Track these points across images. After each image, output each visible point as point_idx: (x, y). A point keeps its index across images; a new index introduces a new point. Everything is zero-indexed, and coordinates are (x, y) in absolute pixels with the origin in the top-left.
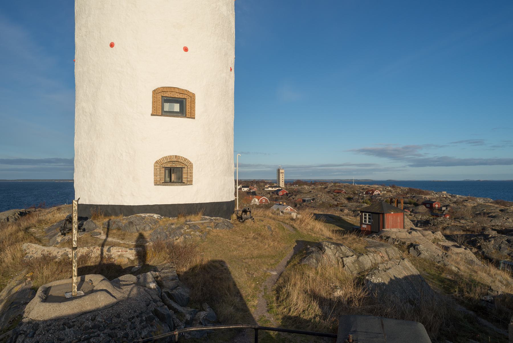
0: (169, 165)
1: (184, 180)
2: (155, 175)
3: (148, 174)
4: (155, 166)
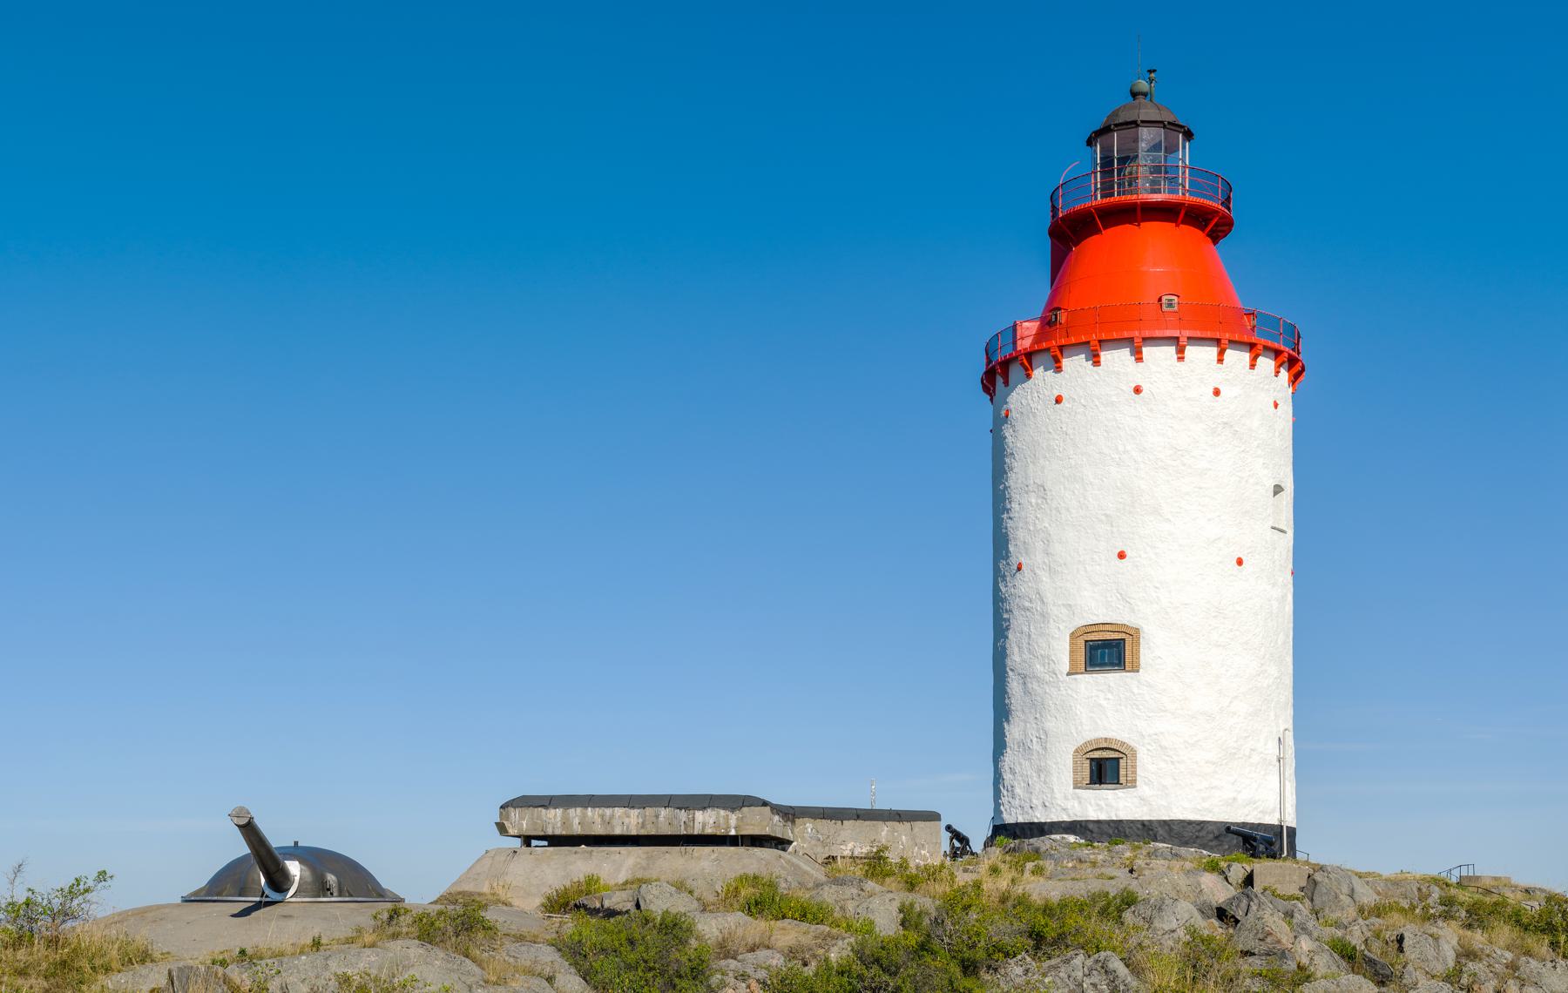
0: (1097, 755)
1: (1122, 779)
2: (1075, 772)
3: (1098, 608)
4: (1075, 757)
